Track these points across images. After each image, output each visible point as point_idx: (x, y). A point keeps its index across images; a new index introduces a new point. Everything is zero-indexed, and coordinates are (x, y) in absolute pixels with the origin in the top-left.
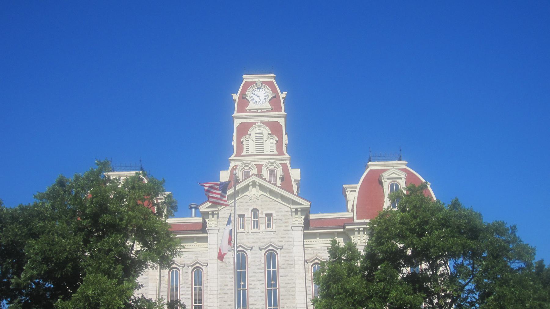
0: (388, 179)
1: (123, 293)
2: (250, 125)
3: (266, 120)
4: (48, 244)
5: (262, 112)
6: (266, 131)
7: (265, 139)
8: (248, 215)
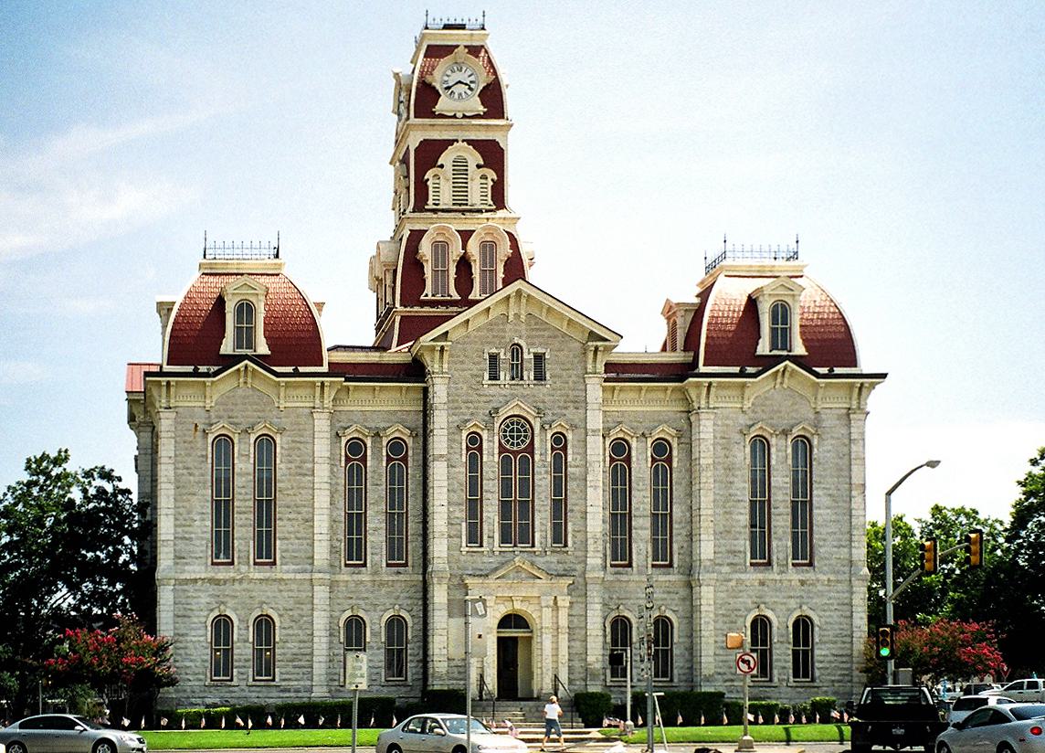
6: (474, 158)
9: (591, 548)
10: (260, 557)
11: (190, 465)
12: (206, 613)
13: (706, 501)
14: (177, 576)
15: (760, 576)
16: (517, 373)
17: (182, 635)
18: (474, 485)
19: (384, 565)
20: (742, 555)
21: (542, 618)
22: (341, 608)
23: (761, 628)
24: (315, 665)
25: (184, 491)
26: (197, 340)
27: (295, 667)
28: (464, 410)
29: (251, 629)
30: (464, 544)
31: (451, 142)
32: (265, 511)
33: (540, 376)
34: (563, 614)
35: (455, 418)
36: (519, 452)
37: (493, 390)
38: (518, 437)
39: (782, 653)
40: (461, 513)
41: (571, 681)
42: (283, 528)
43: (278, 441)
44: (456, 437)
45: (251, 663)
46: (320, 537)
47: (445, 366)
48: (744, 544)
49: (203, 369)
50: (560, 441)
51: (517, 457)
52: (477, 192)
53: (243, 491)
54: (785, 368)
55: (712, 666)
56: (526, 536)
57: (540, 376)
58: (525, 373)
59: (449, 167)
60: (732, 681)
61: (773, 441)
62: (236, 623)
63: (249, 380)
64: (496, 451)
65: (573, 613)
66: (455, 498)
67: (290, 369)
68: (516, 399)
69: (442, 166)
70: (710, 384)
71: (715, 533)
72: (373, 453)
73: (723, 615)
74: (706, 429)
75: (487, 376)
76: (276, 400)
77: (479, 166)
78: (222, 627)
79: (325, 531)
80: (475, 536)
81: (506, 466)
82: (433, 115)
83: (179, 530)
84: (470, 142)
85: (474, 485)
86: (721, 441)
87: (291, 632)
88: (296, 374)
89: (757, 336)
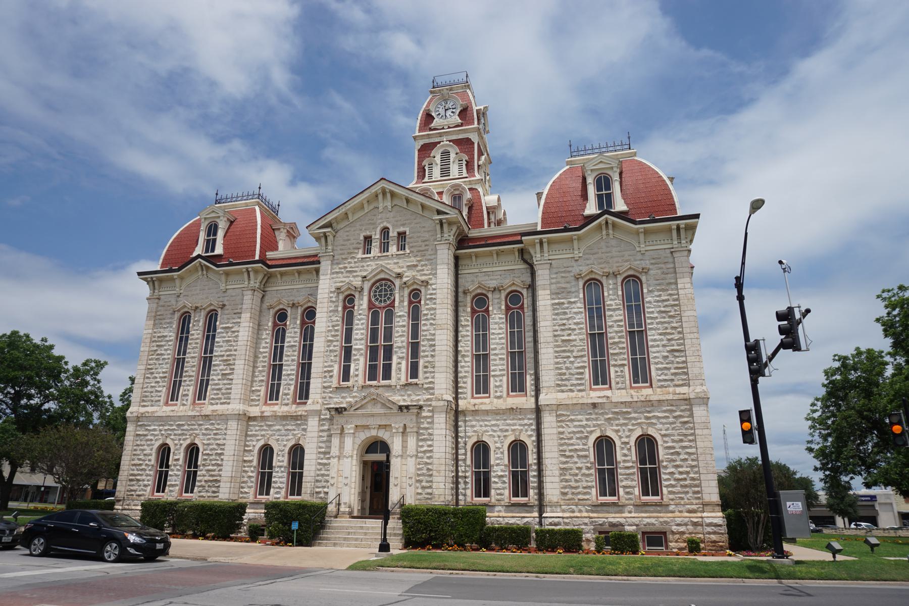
0: (592, 170)
1: (841, 474)
2: (435, 145)
3: (454, 137)
4: (402, 411)
5: (449, 128)
6: (453, 151)
7: (451, 160)
8: (376, 236)
38: (385, 295)
63: (611, 232)
82: (431, 130)
89: (585, 196)
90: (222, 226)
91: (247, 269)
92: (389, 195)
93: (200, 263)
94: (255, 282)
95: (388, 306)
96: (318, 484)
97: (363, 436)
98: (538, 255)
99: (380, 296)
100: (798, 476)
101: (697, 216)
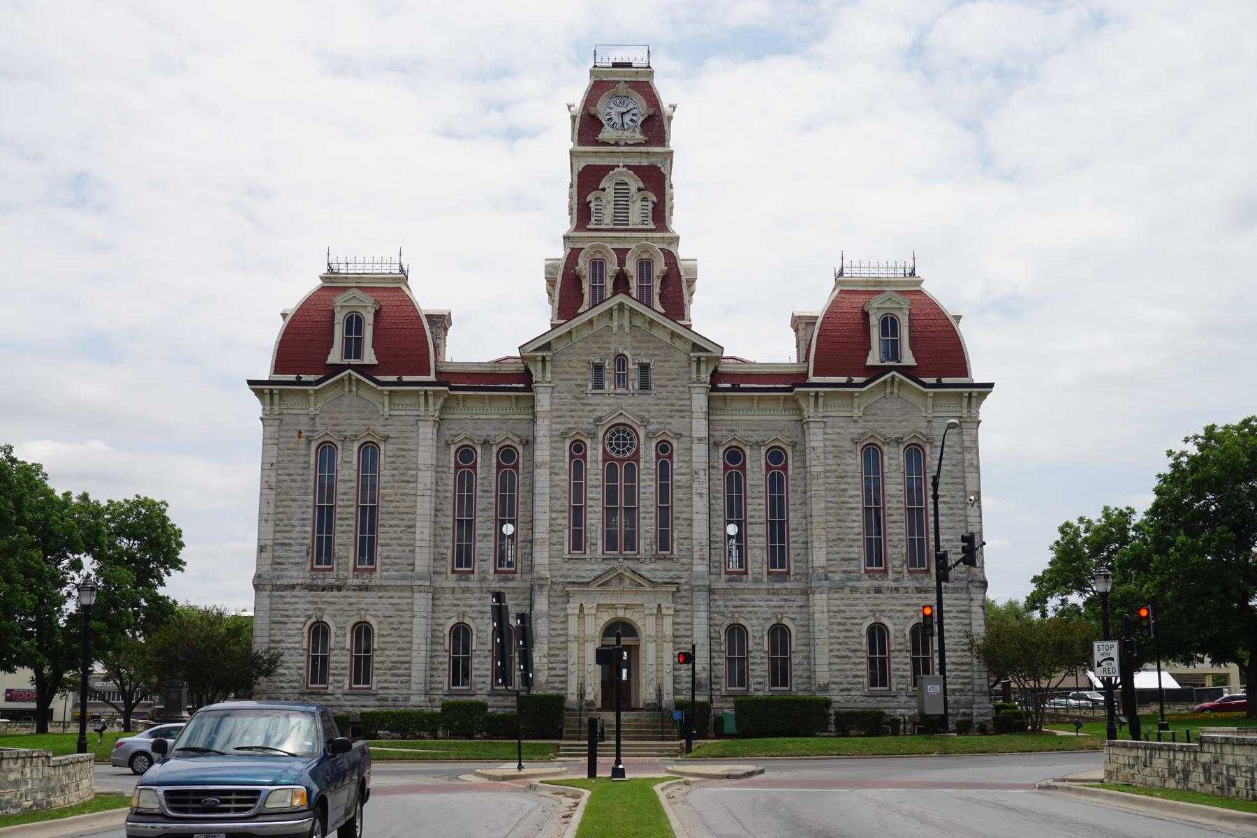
5: (627, 145)
6: (634, 183)
9: (696, 556)
10: (459, 565)
11: (291, 472)
12: (303, 619)
13: (818, 507)
14: (274, 582)
15: (875, 583)
16: (621, 380)
17: (278, 642)
18: (578, 490)
19: (492, 571)
20: (856, 563)
21: (646, 626)
22: (447, 615)
23: (878, 635)
24: (413, 673)
25: (284, 497)
26: (306, 348)
27: (393, 675)
28: (568, 419)
29: (349, 636)
30: (566, 551)
31: (613, 167)
32: (368, 515)
33: (645, 385)
34: (668, 622)
35: (559, 426)
36: (624, 460)
37: (597, 400)
38: (624, 445)
39: (900, 663)
40: (564, 521)
41: (676, 691)
42: (383, 535)
43: (382, 448)
44: (559, 445)
45: (348, 672)
46: (422, 543)
47: (549, 375)
48: (858, 551)
49: (305, 378)
50: (664, 448)
51: (621, 469)
52: (637, 212)
53: (345, 497)
54: (893, 377)
55: (827, 675)
56: (631, 541)
57: (645, 385)
58: (630, 383)
59: (610, 193)
60: (849, 690)
61: (885, 449)
62: (333, 629)
63: (896, 390)
64: (600, 458)
65: (678, 620)
66: (557, 505)
67: (394, 378)
68: (612, 404)
69: (604, 190)
70: (970, 394)
71: (828, 540)
72: (483, 460)
73: (839, 624)
74: (816, 438)
75: (590, 386)
76: (380, 406)
77: (639, 190)
78: (319, 632)
79: (427, 537)
80: (578, 541)
81: (611, 472)
82: (597, 143)
83: (278, 535)
84: (630, 167)
85: (578, 490)
86: (831, 449)
87: (389, 639)
88: (400, 383)
89: (867, 348)
90: (369, 319)
91: (426, 392)
92: (627, 313)
93: (350, 375)
94: (433, 409)
95: (629, 459)
96: (553, 673)
97: (606, 617)
98: (812, 411)
99: (618, 445)
100: (1141, 502)
101: (991, 385)
